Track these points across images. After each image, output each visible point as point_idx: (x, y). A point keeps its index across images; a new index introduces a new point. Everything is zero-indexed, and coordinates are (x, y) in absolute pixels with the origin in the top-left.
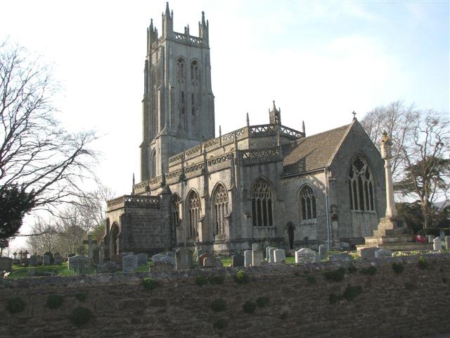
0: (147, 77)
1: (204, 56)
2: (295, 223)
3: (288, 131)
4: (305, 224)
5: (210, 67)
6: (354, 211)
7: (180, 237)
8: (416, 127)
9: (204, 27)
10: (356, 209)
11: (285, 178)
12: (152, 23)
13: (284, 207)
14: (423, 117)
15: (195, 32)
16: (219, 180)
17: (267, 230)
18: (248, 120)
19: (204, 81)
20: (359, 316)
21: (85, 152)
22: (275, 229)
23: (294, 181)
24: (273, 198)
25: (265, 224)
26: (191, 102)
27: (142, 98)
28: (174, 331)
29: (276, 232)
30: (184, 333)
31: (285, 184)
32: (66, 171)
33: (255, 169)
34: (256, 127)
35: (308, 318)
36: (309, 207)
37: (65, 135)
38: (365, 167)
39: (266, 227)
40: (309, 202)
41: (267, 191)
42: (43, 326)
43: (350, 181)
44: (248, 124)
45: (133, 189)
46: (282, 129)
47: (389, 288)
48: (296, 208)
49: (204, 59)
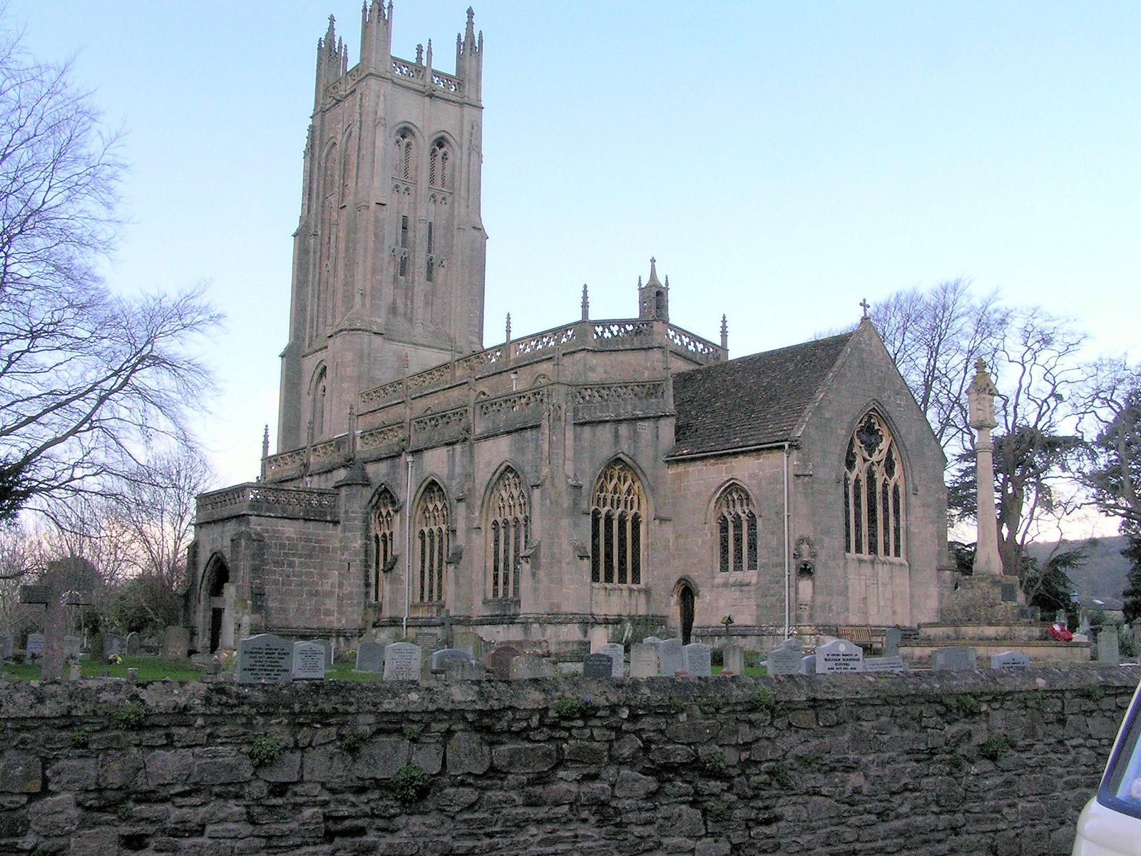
0: (311, 172)
1: (467, 127)
2: (697, 581)
3: (686, 340)
4: (725, 585)
5: (480, 155)
6: (853, 555)
7: (393, 602)
8: (996, 350)
9: (470, 48)
10: (859, 550)
11: (678, 461)
12: (331, 28)
13: (671, 537)
14: (1016, 324)
15: (445, 62)
16: (507, 456)
17: (626, 593)
18: (585, 305)
19: (463, 193)
20: (1009, 806)
21: (158, 361)
22: (647, 592)
23: (699, 471)
24: (645, 513)
25: (622, 579)
26: (426, 244)
27: (295, 225)
28: (616, 825)
29: (648, 602)
30: (638, 830)
31: (679, 477)
32: (104, 412)
33: (605, 433)
34: (606, 324)
35: (901, 805)
36: (738, 540)
37: (104, 313)
38: (884, 445)
39: (623, 586)
40: (738, 526)
41: (629, 492)
42: (325, 804)
43: (846, 479)
44: (585, 313)
45: (264, 467)
46: (672, 333)
47: (1074, 742)
48: (704, 542)
49: (466, 135)
